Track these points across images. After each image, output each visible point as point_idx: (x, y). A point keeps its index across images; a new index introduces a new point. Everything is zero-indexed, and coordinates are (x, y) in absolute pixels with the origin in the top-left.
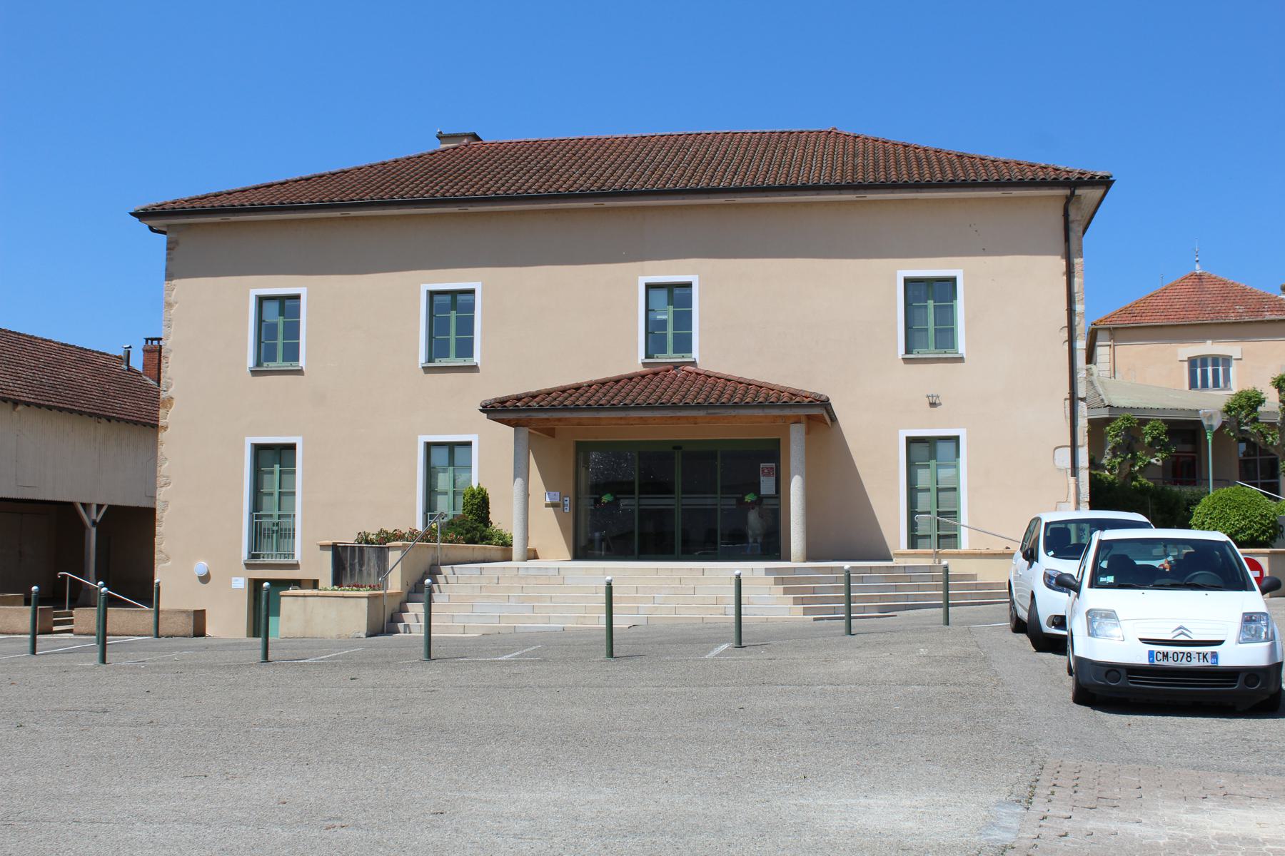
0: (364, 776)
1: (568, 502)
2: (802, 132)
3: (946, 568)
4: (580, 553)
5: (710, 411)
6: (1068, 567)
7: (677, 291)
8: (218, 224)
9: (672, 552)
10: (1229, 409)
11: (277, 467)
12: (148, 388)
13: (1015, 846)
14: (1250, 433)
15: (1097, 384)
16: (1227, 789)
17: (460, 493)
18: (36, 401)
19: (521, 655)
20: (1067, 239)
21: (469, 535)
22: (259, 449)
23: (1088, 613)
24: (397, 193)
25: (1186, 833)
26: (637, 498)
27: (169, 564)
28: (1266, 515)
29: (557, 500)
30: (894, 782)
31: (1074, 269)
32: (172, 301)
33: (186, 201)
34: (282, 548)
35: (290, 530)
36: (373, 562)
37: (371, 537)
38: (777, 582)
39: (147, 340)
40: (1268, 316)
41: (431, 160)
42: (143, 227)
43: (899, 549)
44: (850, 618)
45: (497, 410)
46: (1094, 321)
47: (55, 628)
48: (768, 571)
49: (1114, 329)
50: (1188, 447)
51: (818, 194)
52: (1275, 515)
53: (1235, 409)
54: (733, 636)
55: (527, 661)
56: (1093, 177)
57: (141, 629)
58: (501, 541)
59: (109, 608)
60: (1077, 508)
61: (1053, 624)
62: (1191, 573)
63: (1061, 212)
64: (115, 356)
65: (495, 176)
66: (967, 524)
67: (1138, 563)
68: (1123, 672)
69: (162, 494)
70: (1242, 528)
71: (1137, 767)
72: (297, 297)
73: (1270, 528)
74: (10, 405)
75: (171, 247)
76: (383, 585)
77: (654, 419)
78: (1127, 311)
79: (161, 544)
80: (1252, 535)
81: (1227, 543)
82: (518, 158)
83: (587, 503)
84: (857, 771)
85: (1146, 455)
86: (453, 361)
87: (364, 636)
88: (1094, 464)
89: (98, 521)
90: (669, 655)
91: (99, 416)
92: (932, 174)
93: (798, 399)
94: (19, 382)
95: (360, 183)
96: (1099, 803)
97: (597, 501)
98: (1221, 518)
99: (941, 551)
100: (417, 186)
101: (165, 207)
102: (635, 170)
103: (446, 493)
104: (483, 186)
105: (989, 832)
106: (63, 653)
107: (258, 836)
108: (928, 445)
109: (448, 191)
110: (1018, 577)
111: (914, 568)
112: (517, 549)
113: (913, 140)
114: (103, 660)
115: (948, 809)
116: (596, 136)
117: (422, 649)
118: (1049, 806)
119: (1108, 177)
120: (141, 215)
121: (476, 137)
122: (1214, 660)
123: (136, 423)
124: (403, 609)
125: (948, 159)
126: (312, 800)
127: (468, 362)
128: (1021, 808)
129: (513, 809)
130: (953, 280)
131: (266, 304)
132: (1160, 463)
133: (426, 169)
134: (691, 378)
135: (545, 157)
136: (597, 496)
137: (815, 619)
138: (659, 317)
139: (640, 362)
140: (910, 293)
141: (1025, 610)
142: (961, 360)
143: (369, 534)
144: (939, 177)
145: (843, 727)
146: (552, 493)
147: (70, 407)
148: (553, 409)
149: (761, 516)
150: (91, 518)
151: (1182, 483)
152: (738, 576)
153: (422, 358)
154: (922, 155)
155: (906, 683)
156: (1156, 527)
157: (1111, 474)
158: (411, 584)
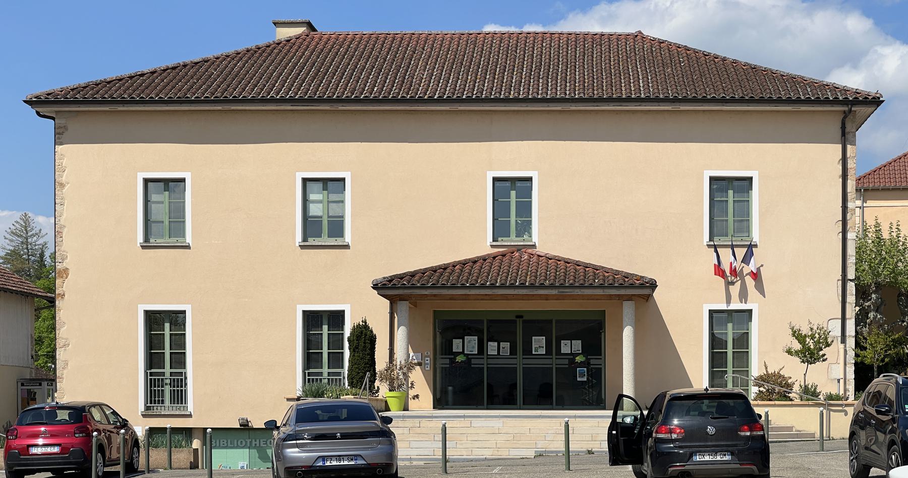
1: (428, 362)
5: (561, 290)
9: (483, 405)
42: (31, 111)
63: (840, 125)
79: (64, 397)
119: (879, 98)
127: (339, 242)
136: (453, 356)
139: (489, 244)
142: (188, 247)
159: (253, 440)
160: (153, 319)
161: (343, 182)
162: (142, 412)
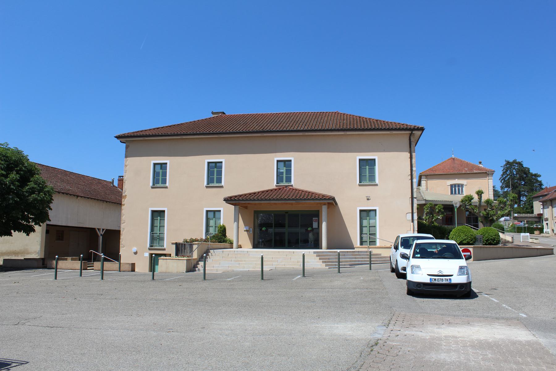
0: (181, 316)
1: (251, 230)
2: (327, 112)
3: (370, 252)
4: (255, 246)
6: (406, 251)
7: (287, 163)
8: (142, 140)
9: (272, 246)
10: (462, 201)
11: (159, 218)
12: (119, 192)
13: (382, 339)
14: (469, 209)
15: (421, 193)
16: (450, 321)
17: (217, 227)
18: (84, 196)
19: (234, 279)
20: (410, 147)
21: (219, 240)
22: (153, 212)
23: (412, 266)
24: (198, 131)
25: (435, 335)
27: (124, 248)
28: (472, 235)
29: (248, 229)
30: (347, 319)
31: (412, 156)
32: (127, 165)
33: (132, 133)
34: (160, 244)
35: (163, 238)
36: (188, 249)
37: (188, 240)
38: (317, 256)
39: (119, 176)
40: (475, 172)
41: (209, 120)
42: (118, 141)
43: (357, 245)
44: (339, 268)
45: (229, 200)
46: (421, 173)
47: (88, 268)
48: (314, 252)
49: (427, 175)
50: (450, 213)
51: (332, 132)
52: (475, 235)
53: (464, 201)
54: (302, 273)
55: (236, 281)
56: (418, 128)
57: (115, 269)
58: (229, 242)
59: (104, 262)
60: (414, 233)
61: (403, 270)
62: (444, 253)
63: (408, 139)
64: (109, 182)
65: (229, 126)
66: (378, 238)
67: (429, 250)
68: (422, 285)
69: (122, 226)
70: (465, 239)
71: (423, 314)
72: (166, 164)
73: (474, 239)
74: (76, 197)
75: (127, 147)
76: (191, 256)
77: (279, 203)
78: (431, 170)
80: (468, 241)
81: (455, 244)
82: (237, 120)
83: (257, 230)
84: (336, 316)
85: (437, 215)
86: (215, 184)
87: (185, 272)
88: (419, 218)
89: (102, 234)
90: (281, 279)
91: (104, 201)
92: (368, 126)
93: (325, 197)
94: (79, 190)
95: (187, 128)
96: (411, 325)
97: (261, 230)
98: (458, 236)
99: (370, 246)
100: (205, 128)
101: (125, 135)
102: (274, 124)
103: (212, 227)
104: (225, 129)
105: (374, 335)
106: (90, 276)
107: (146, 334)
108: (366, 212)
109: (214, 130)
110: (393, 255)
111: (361, 252)
112: (235, 245)
113: (362, 115)
114: (102, 279)
115: (362, 328)
116: (262, 113)
117: (203, 276)
118: (394, 327)
119: (423, 128)
120: (118, 137)
121: (224, 113)
122: (450, 281)
123: (115, 203)
124: (198, 264)
125: (373, 121)
126: (164, 323)
127: (220, 185)
128: (385, 327)
129: (226, 327)
130: (374, 160)
131: (156, 166)
132: (441, 218)
133: (208, 123)
134: (291, 190)
135: (246, 119)
136: (261, 228)
137: (329, 268)
138: (281, 171)
139: (275, 185)
140: (361, 164)
141: (394, 265)
142: (377, 185)
143: (187, 240)
144: (370, 127)
145: (333, 302)
146: (246, 227)
147: (94, 198)
148: (247, 200)
149: (313, 235)
150: (100, 233)
151: (448, 225)
152: (304, 254)
153: (205, 183)
154: (365, 120)
155: (355, 289)
156: (436, 239)
157: (426, 222)
158: (200, 256)
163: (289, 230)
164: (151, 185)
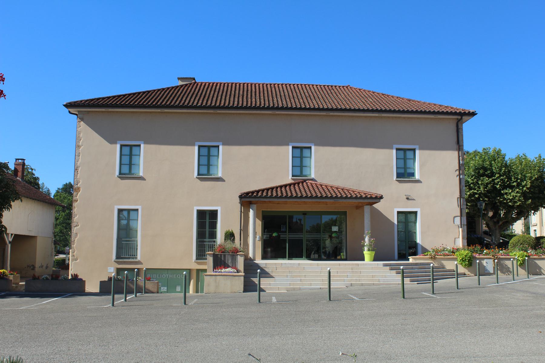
26: (287, 235)
38: (391, 269)
42: (66, 110)
51: (364, 113)
77: (310, 202)
87: (242, 292)
120: (68, 106)
136: (271, 234)
159: (170, 275)
160: (201, 214)
161: (310, 150)
162: (114, 260)
163: (318, 236)
164: (118, 175)
